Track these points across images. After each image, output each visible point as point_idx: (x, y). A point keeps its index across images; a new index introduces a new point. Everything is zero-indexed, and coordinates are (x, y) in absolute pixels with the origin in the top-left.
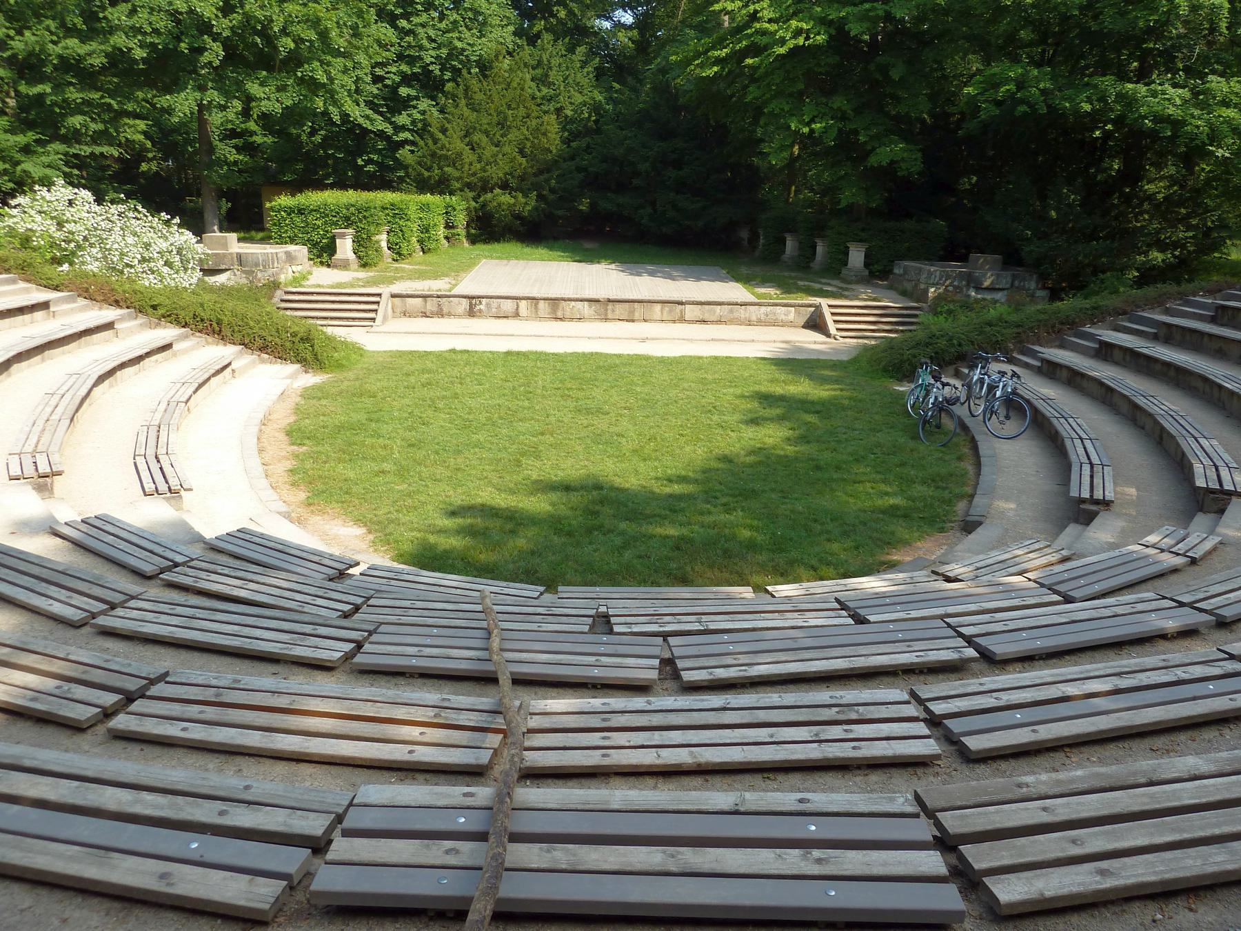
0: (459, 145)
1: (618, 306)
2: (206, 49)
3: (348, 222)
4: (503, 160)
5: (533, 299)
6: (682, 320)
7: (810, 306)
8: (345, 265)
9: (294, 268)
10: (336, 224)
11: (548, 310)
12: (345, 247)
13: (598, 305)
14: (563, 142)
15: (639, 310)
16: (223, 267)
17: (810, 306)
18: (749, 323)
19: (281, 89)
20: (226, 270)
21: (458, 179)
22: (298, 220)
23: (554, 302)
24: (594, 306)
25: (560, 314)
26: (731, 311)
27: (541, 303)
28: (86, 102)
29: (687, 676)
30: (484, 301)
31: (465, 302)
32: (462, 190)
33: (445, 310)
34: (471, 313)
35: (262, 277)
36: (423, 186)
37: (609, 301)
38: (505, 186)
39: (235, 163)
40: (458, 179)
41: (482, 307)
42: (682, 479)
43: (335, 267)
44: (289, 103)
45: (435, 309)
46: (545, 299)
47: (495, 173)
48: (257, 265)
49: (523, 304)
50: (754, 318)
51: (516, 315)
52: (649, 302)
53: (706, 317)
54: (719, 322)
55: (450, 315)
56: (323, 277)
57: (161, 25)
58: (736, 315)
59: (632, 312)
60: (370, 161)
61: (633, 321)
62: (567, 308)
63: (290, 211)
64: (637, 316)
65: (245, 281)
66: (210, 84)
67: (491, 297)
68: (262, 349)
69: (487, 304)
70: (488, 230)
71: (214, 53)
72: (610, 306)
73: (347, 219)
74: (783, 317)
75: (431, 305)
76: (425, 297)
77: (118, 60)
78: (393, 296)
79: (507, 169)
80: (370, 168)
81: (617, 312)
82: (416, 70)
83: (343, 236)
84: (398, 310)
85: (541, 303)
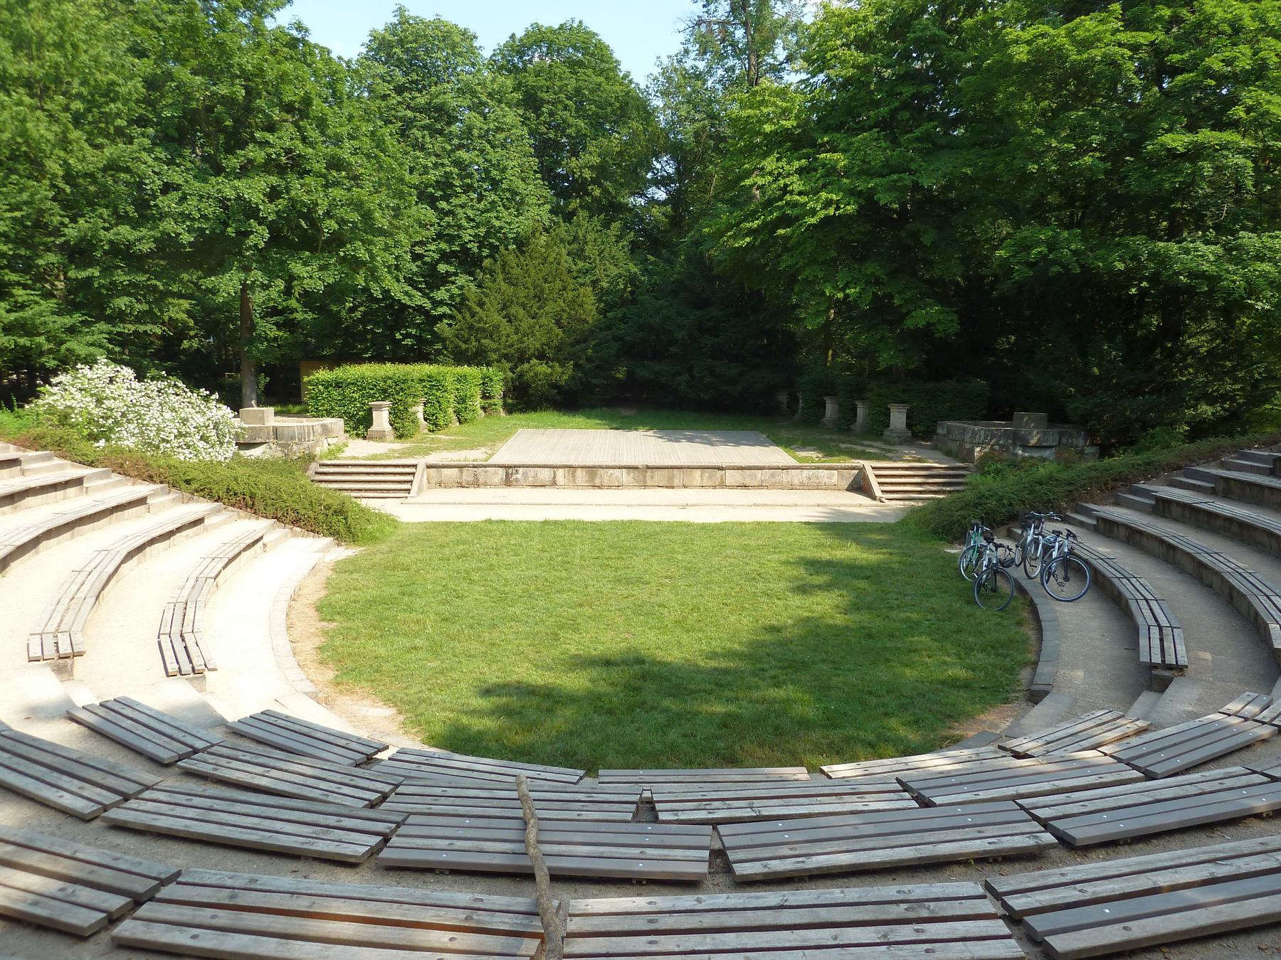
0: (497, 318)
1: (657, 472)
2: (252, 233)
3: (385, 394)
4: (540, 330)
6: (722, 485)
7: (854, 468)
8: (381, 437)
9: (330, 441)
10: (372, 396)
13: (636, 472)
15: (659, 476)
16: (259, 441)
17: (854, 468)
21: (495, 351)
22: (335, 393)
23: (592, 470)
25: (597, 482)
26: (773, 475)
28: (131, 284)
30: (521, 470)
31: (501, 472)
32: (499, 361)
34: (508, 482)
36: (461, 358)
37: (648, 467)
38: (541, 356)
40: (495, 351)
41: (519, 476)
43: (371, 438)
44: (331, 281)
45: (471, 479)
47: (533, 344)
48: (293, 438)
49: (560, 472)
50: (796, 482)
51: (554, 483)
52: (689, 468)
53: (747, 482)
54: (760, 486)
55: (485, 484)
56: (359, 449)
58: (778, 479)
59: (671, 478)
60: (408, 335)
62: (605, 476)
63: (327, 385)
65: (279, 454)
68: (295, 522)
70: (524, 399)
71: (260, 235)
72: (649, 473)
73: (384, 391)
75: (467, 475)
77: (166, 244)
78: (429, 467)
80: (408, 342)
81: (656, 478)
83: (379, 408)
84: (434, 481)
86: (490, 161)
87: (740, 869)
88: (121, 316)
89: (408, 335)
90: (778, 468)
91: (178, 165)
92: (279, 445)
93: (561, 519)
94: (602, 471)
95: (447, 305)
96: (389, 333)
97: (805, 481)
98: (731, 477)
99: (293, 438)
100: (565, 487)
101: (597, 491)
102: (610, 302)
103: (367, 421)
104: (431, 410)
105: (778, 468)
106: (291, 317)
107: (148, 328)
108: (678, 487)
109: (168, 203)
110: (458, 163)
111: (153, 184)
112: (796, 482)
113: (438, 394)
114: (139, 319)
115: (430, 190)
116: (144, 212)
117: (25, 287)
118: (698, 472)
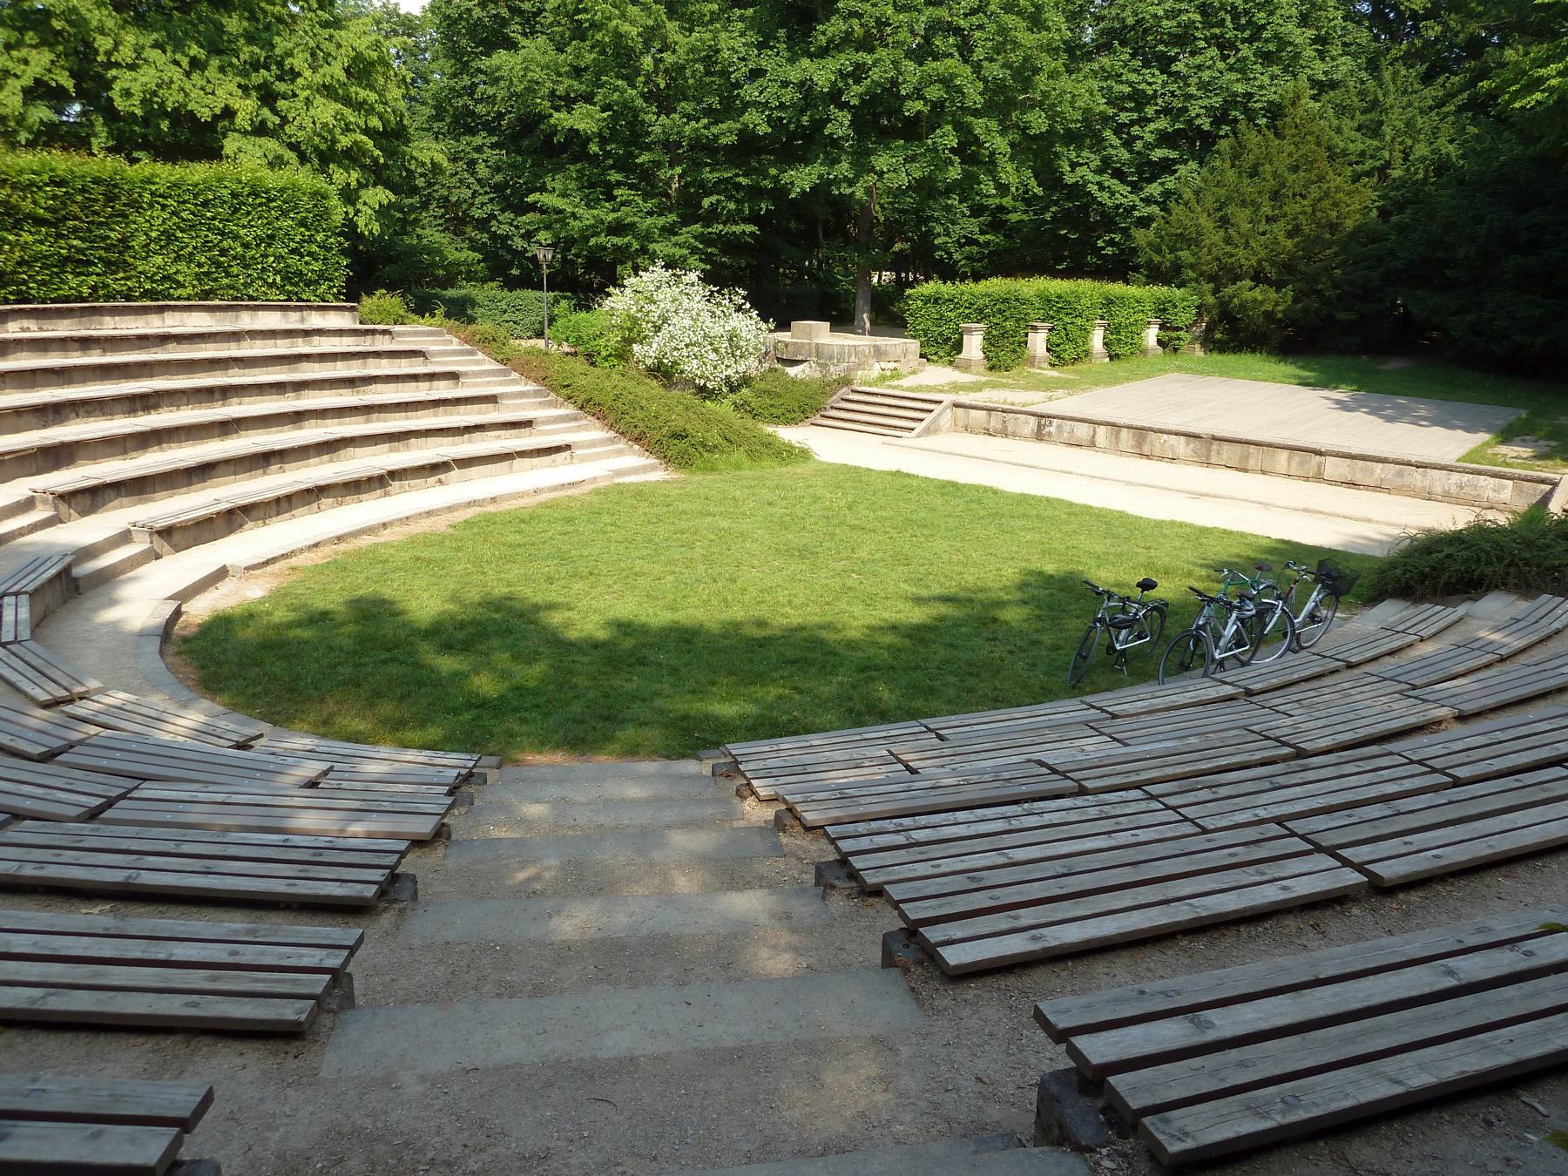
0: (1206, 223)
1: (1226, 446)
2: (830, 120)
3: (981, 315)
4: (1264, 237)
5: (1114, 425)
6: (1319, 478)
7: (1543, 481)
8: (966, 367)
9: (884, 365)
10: (967, 317)
11: (1132, 442)
12: (974, 345)
14: (1381, 210)
15: (1228, 451)
16: (800, 358)
17: (1543, 481)
18: (1429, 497)
19: (911, 159)
20: (802, 361)
21: (1192, 266)
22: (932, 310)
23: (1141, 431)
24: (1194, 444)
25: (1146, 449)
26: (1400, 474)
28: (720, 181)
29: (954, 956)
30: (1055, 421)
31: (1033, 421)
32: (1197, 281)
34: (1039, 436)
35: (835, 371)
36: (1157, 275)
37: (1214, 438)
38: (1258, 278)
39: (987, 243)
40: (1192, 266)
41: (1052, 429)
42: (131, 579)
43: (957, 367)
44: (918, 174)
47: (1245, 258)
48: (831, 358)
49: (1102, 430)
50: (1438, 489)
52: (1270, 445)
53: (1358, 478)
54: (1378, 488)
55: (1014, 435)
56: (937, 375)
57: (786, 99)
58: (1407, 480)
59: (1246, 458)
60: (1111, 243)
61: (1246, 471)
62: (1157, 443)
64: (1251, 464)
65: (818, 375)
68: (637, 440)
69: (1059, 427)
70: (1232, 334)
71: (840, 124)
74: (1491, 494)
75: (995, 421)
76: (989, 410)
77: (747, 136)
78: (957, 405)
79: (1263, 254)
80: (1109, 251)
81: (1224, 456)
82: (1178, 126)
83: (970, 331)
84: (960, 423)
85: (1124, 433)
88: (712, 216)
89: (1111, 243)
90: (1409, 464)
91: (771, 48)
92: (819, 364)
94: (1153, 435)
96: (1066, 239)
97: (1454, 490)
98: (1332, 467)
99: (831, 358)
100: (1104, 450)
101: (1145, 461)
102: (1403, 202)
104: (1054, 339)
105: (1409, 464)
107: (737, 229)
109: (750, 92)
112: (1438, 489)
114: (731, 218)
115: (1161, 48)
116: (730, 107)
117: (631, 187)
118: (1284, 454)
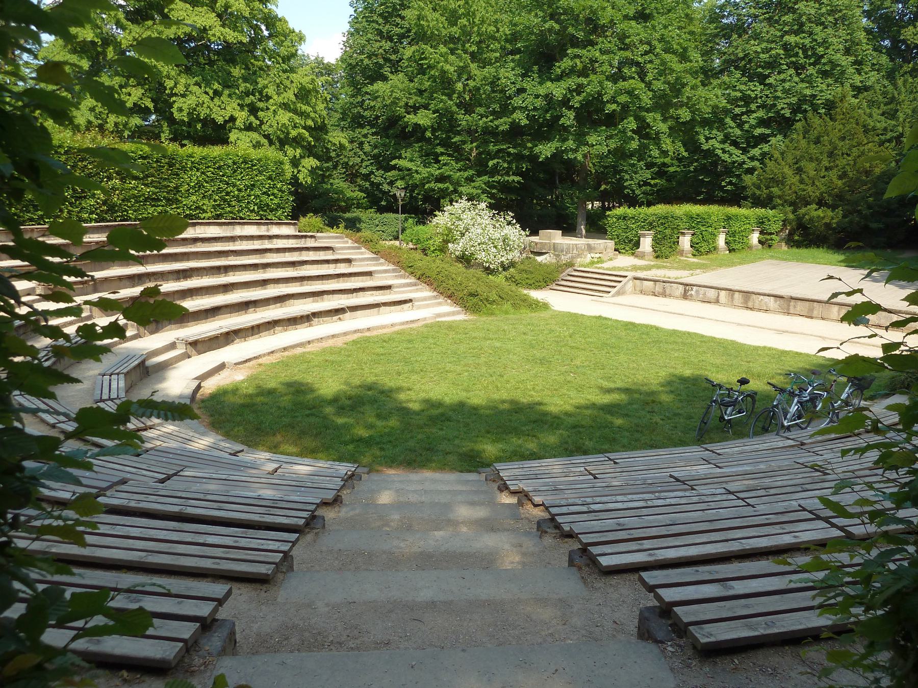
0: (788, 171)
1: (799, 303)
3: (651, 226)
5: (730, 290)
8: (642, 256)
9: (593, 255)
10: (643, 227)
11: (741, 300)
12: (647, 243)
13: (782, 300)
15: (800, 306)
21: (780, 197)
23: (747, 294)
24: (779, 301)
25: (750, 305)
27: (737, 295)
28: (500, 151)
30: (695, 288)
31: (681, 288)
33: (668, 292)
34: (685, 296)
35: (564, 259)
36: (758, 202)
37: (792, 298)
38: (821, 203)
39: (656, 185)
40: (780, 197)
41: (693, 293)
43: (636, 256)
45: (661, 291)
46: (739, 291)
47: (812, 192)
48: (562, 251)
49: (723, 293)
51: (717, 301)
55: (670, 296)
59: (811, 310)
60: (730, 183)
61: (812, 318)
62: (756, 301)
63: (619, 218)
64: (815, 313)
65: (554, 261)
66: (570, 137)
67: (700, 286)
68: (450, 297)
71: (568, 118)
72: (792, 303)
73: (651, 224)
75: (659, 288)
76: (655, 281)
78: (636, 279)
79: (823, 189)
80: (729, 188)
81: (798, 308)
83: (644, 235)
84: (638, 289)
85: (737, 295)
86: (816, 40)
87: (605, 561)
88: (494, 171)
89: (730, 183)
91: (529, 77)
93: (637, 322)
95: (757, 159)
100: (725, 305)
101: (749, 312)
103: (637, 244)
106: (666, 169)
108: (817, 318)
109: (517, 101)
110: (786, 47)
111: (511, 90)
113: (703, 228)
115: (760, 70)
116: (506, 110)
